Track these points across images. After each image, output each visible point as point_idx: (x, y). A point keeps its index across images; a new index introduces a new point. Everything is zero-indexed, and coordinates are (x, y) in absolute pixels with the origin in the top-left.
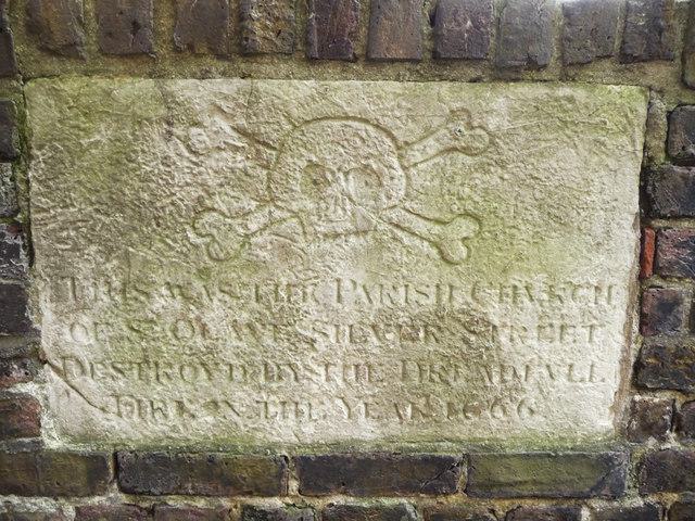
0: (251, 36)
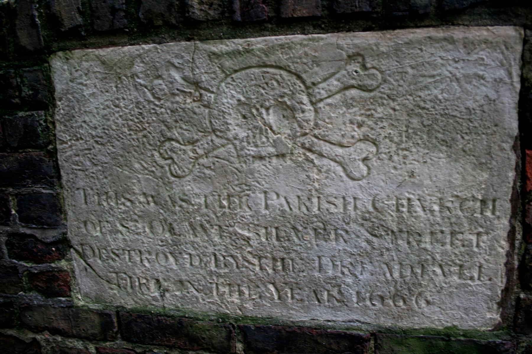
0: (191, 10)
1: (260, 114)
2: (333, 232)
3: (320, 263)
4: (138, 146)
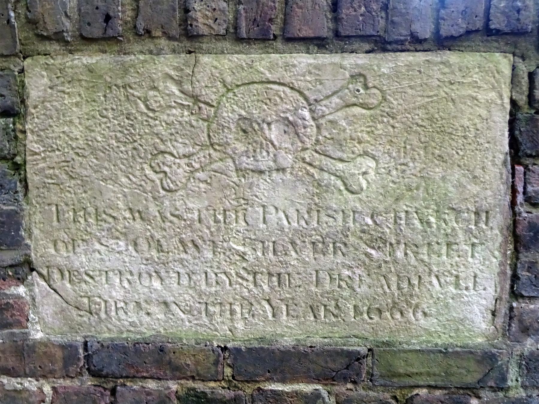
1: (262, 129)
2: (331, 245)
3: (317, 276)
4: (126, 159)
